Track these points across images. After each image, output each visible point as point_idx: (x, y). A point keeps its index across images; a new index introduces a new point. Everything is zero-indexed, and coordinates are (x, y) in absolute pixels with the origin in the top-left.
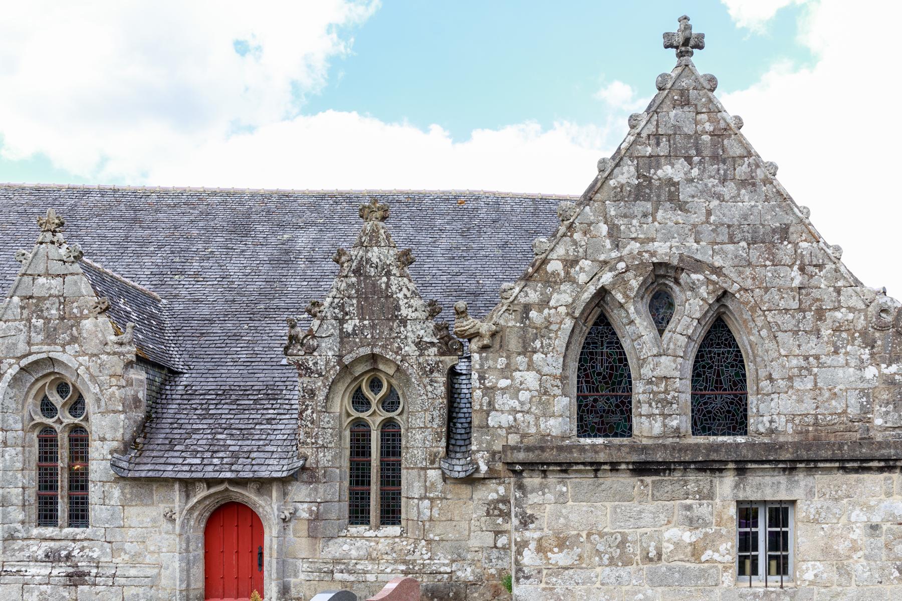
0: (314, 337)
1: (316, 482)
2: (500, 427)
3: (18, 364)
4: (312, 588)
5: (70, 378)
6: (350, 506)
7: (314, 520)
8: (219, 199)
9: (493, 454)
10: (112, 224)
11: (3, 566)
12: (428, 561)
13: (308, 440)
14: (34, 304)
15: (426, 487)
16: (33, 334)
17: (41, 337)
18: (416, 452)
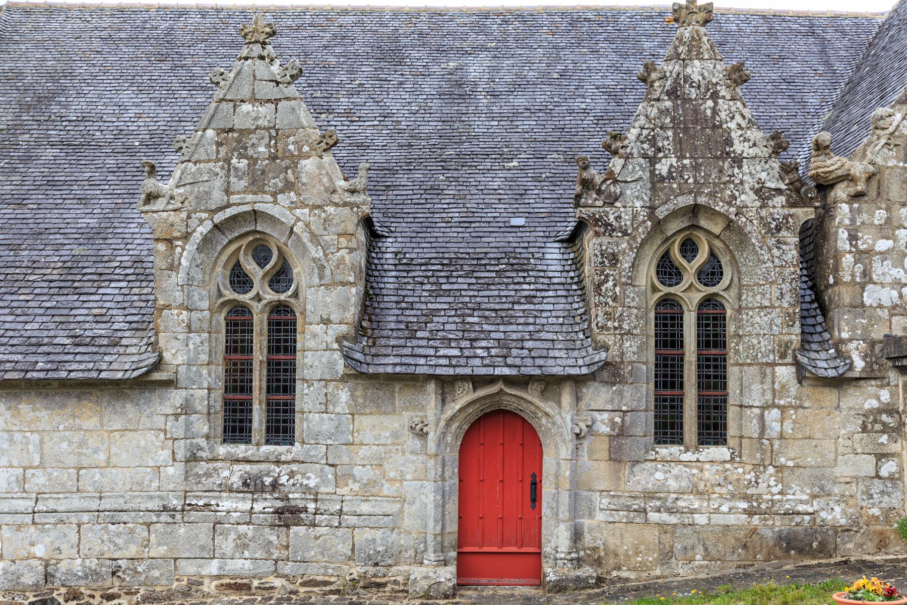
0: (616, 182)
1: (620, 382)
2: (880, 306)
3: (212, 220)
4: (618, 533)
5: (277, 237)
6: (656, 417)
7: (618, 436)
8: (353, 19)
9: (872, 344)
10: (222, 51)
11: (185, 497)
12: (779, 497)
13: (609, 324)
14: (234, 139)
15: (774, 390)
16: (233, 180)
17: (243, 183)
18: (755, 341)
